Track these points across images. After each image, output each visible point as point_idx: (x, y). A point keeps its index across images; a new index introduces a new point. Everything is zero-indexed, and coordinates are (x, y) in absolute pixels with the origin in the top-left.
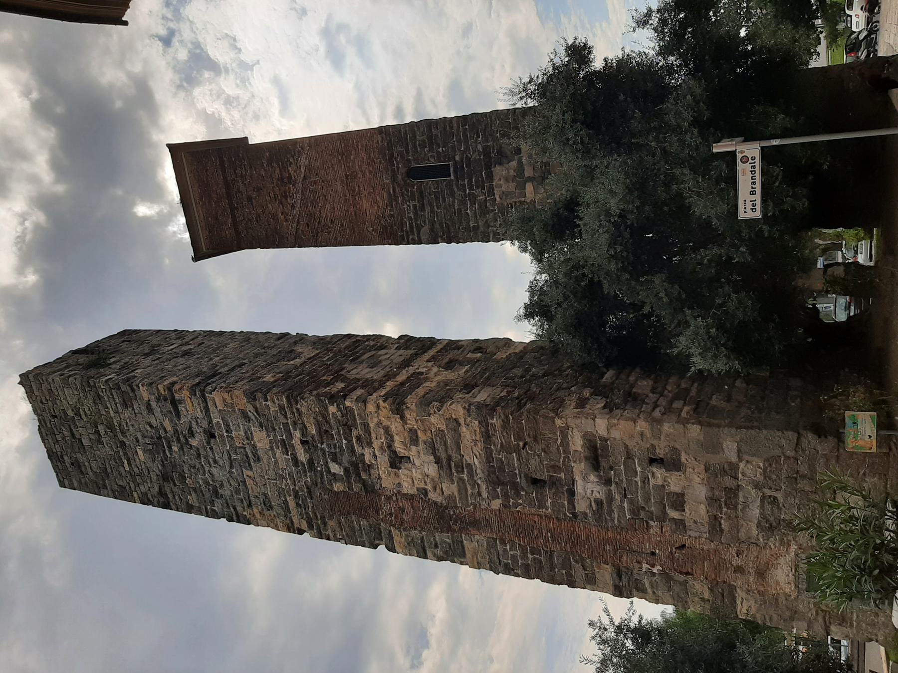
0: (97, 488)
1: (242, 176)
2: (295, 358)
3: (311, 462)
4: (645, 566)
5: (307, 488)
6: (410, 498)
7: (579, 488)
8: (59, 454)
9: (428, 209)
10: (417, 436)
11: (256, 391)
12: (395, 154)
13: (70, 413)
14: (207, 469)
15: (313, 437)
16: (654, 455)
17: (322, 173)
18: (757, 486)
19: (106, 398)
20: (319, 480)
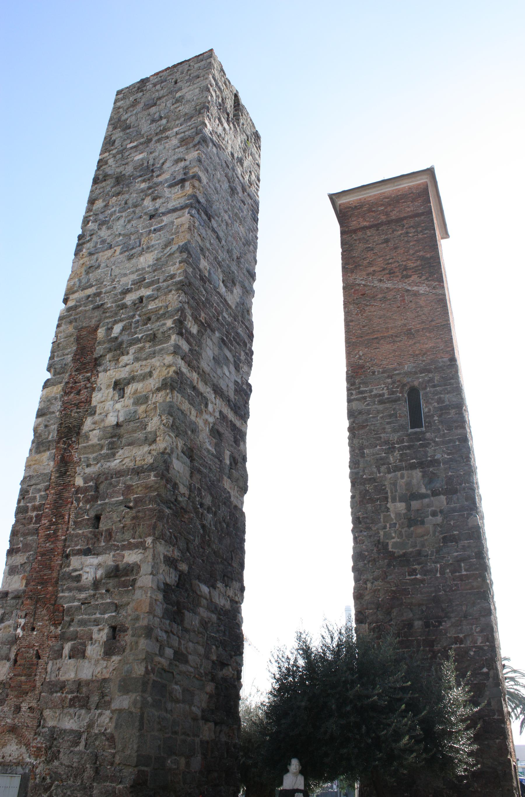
0: (117, 123)
1: (407, 233)
2: (226, 286)
3: (124, 306)
4: (22, 621)
5: (102, 305)
6: (89, 401)
7: (93, 560)
8: (144, 88)
9: (380, 407)
10: (141, 404)
11: (189, 253)
12: (431, 375)
13: (179, 94)
14: (123, 214)
15: (146, 306)
16: (119, 631)
18: (90, 725)
19: (189, 124)
20: (107, 315)
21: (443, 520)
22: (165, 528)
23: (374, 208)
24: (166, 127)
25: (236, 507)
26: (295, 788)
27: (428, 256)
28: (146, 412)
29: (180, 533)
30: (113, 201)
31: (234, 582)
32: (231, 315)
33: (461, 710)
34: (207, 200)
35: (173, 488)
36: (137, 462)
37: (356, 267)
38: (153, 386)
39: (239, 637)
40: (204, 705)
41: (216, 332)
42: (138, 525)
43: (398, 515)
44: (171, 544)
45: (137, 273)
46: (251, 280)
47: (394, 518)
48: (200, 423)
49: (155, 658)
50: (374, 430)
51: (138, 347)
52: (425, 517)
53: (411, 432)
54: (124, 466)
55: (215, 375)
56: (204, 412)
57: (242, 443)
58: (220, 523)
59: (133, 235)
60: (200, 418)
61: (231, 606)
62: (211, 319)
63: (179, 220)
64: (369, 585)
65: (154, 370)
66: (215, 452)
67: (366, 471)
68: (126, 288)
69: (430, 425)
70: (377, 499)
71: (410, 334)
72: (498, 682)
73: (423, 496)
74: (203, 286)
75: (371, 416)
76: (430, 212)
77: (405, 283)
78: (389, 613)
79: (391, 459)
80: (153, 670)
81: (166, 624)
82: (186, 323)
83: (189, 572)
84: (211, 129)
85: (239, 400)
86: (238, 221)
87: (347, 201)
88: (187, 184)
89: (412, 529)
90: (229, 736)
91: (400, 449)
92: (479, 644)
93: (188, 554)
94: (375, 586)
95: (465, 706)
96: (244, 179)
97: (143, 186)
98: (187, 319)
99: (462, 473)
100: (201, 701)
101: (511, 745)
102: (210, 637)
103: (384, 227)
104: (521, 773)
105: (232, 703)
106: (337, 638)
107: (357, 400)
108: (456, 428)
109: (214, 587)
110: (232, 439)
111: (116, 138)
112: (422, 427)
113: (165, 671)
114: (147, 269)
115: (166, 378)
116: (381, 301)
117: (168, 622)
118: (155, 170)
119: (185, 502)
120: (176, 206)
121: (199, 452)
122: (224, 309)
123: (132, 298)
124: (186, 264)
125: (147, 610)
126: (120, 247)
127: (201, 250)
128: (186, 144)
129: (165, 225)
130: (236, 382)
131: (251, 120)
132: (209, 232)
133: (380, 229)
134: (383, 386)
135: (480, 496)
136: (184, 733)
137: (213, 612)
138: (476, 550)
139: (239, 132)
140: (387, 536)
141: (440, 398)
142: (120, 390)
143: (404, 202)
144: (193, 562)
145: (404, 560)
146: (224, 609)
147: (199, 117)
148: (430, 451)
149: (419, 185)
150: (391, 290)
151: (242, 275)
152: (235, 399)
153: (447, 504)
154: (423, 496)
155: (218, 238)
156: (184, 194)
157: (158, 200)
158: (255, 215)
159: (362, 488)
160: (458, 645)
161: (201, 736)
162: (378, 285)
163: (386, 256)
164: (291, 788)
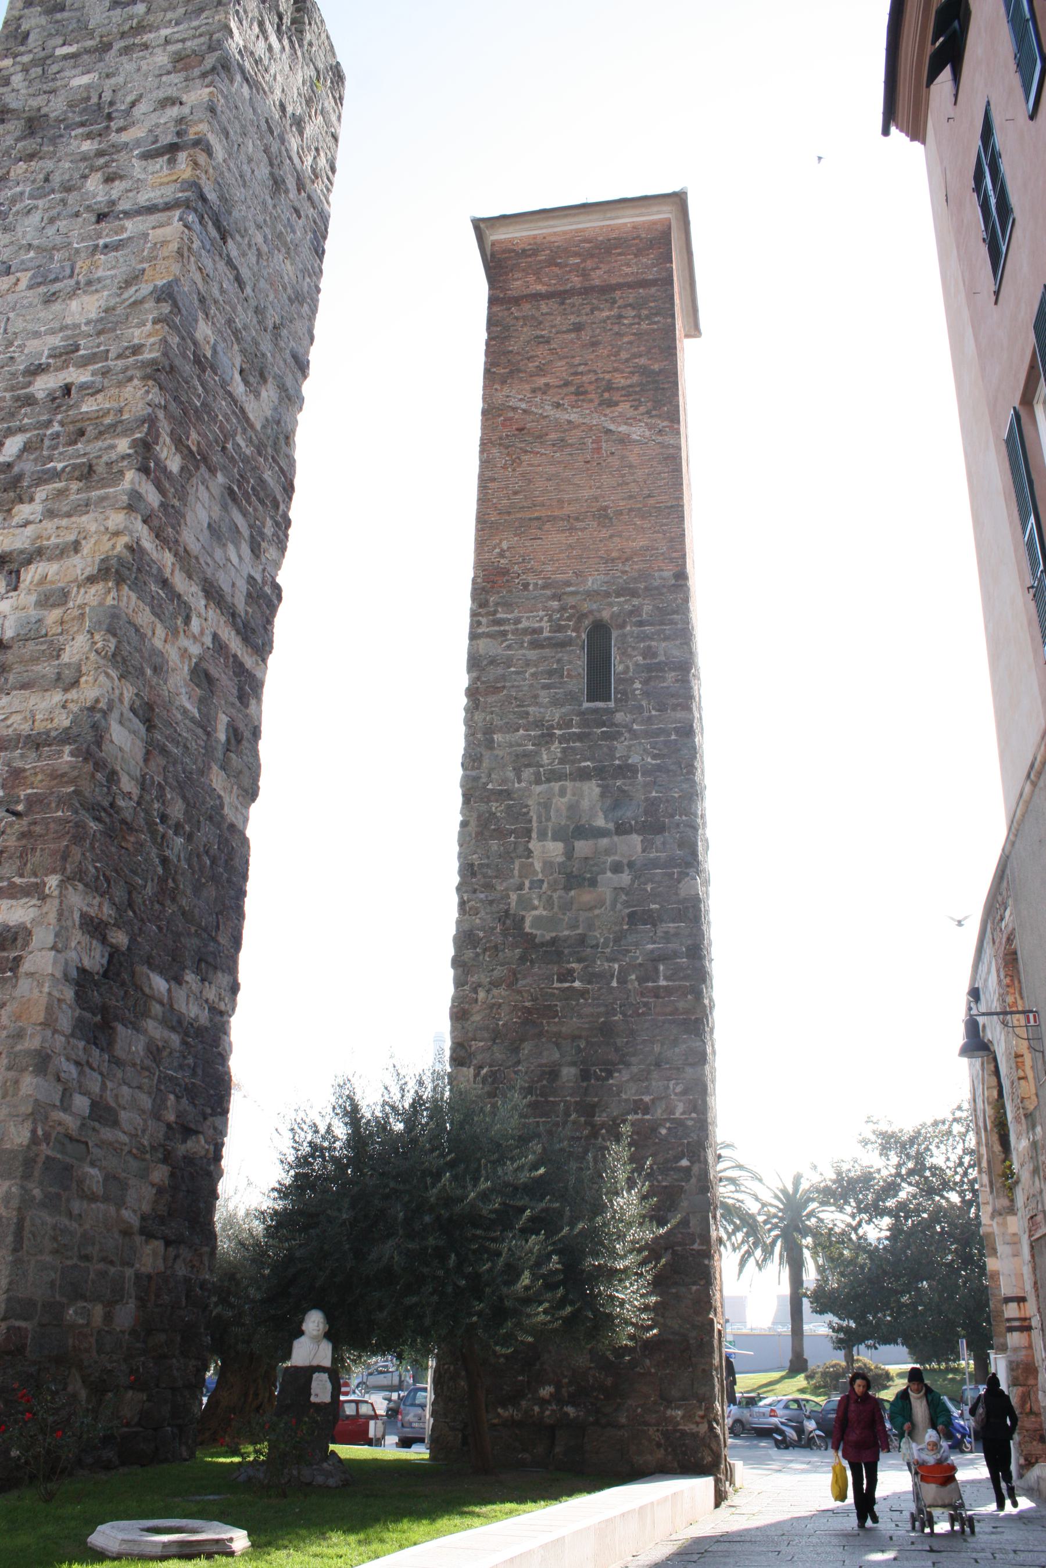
1: (620, 317)
2: (247, 383)
3: (29, 401)
9: (533, 654)
10: (54, 606)
11: (175, 304)
12: (636, 602)
14: (40, 203)
15: (76, 405)
17: (615, 462)
19: (195, 23)
21: (633, 881)
22: (86, 858)
23: (561, 258)
24: (145, 23)
25: (232, 826)
26: (315, 1363)
27: (656, 367)
28: (62, 623)
29: (116, 871)
30: (20, 171)
31: (220, 974)
32: (251, 440)
33: (634, 1233)
34: (222, 198)
35: (107, 781)
36: (36, 724)
37: (512, 372)
38: (79, 572)
39: (223, 1080)
40: (146, 1207)
41: (219, 475)
42: (32, 849)
43: (548, 865)
44: (96, 891)
45: (61, 335)
46: (299, 374)
47: (539, 870)
48: (172, 654)
49: (52, 1114)
50: (516, 698)
51: (54, 489)
52: (598, 874)
53: (587, 709)
54: (10, 730)
55: (209, 560)
56: (182, 633)
57: (253, 702)
58: (198, 856)
59: (58, 250)
60: (173, 644)
61: (211, 1020)
62: (209, 445)
63: (159, 231)
64: (482, 995)
65: (85, 538)
66: (197, 715)
67: (493, 776)
68: (37, 362)
69: (625, 696)
70: (512, 832)
71: (603, 516)
72: (705, 1185)
73: (602, 833)
74: (199, 377)
75: (513, 669)
76: (668, 281)
77: (605, 415)
78: (516, 1050)
79: (545, 757)
80: (47, 1136)
81: (78, 1048)
82: (158, 448)
83: (129, 949)
84: (241, 43)
85: (254, 616)
86: (283, 250)
87: (507, 236)
88: (182, 156)
89: (572, 893)
90: (193, 1267)
91: (563, 739)
92: (677, 1115)
93: (131, 913)
94: (493, 997)
95: (641, 1224)
96: (303, 163)
97: (87, 146)
98: (161, 440)
99: (676, 795)
100: (140, 1199)
101: (718, 1295)
102: (165, 1078)
103: (577, 300)
104: (730, 1342)
105: (202, 1205)
106: (412, 1092)
107: (488, 635)
108: (674, 708)
109: (178, 980)
110: (235, 692)
111: (32, 29)
112: (610, 700)
113: (71, 1139)
114: (84, 328)
115: (107, 557)
116: (554, 445)
117: (81, 1044)
118: (114, 115)
119: (131, 811)
120: (155, 201)
121: (165, 712)
122: (239, 429)
123: (48, 386)
124: (167, 327)
125: (41, 1019)
126: (29, 274)
127: (200, 301)
128: (185, 69)
129: (129, 238)
130: (251, 579)
131: (328, 37)
132: (221, 265)
133: (568, 301)
134: (541, 613)
135: (707, 840)
136: (104, 1259)
137: (173, 1029)
138: (689, 942)
139: (301, 59)
140: (525, 903)
141: (650, 647)
142: (11, 573)
143: (620, 254)
144: (140, 929)
145: (552, 951)
146: (196, 1025)
147: (217, 11)
148: (620, 747)
149: (654, 223)
150: (575, 428)
151: (280, 359)
152: (247, 613)
153: (644, 851)
154: (602, 833)
155: (239, 280)
156: (175, 178)
157: (117, 183)
158: (318, 242)
159: (483, 807)
160: (640, 1116)
161: (137, 1266)
162: (552, 413)
163: (573, 357)
164: (307, 1364)
